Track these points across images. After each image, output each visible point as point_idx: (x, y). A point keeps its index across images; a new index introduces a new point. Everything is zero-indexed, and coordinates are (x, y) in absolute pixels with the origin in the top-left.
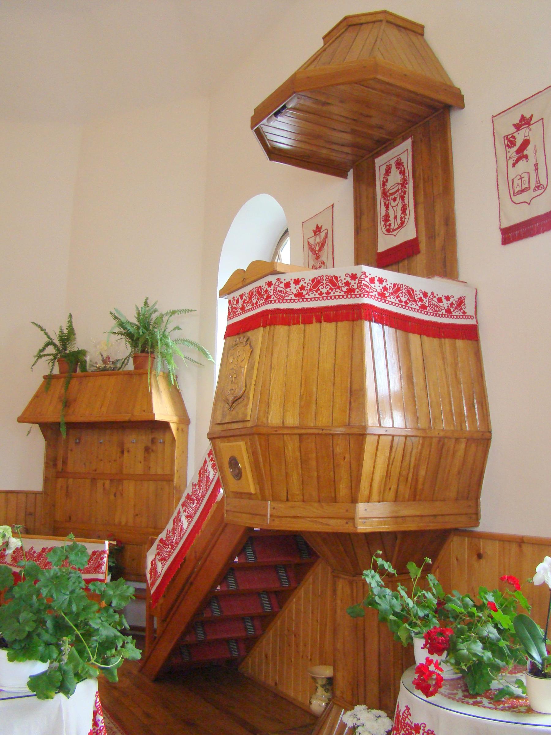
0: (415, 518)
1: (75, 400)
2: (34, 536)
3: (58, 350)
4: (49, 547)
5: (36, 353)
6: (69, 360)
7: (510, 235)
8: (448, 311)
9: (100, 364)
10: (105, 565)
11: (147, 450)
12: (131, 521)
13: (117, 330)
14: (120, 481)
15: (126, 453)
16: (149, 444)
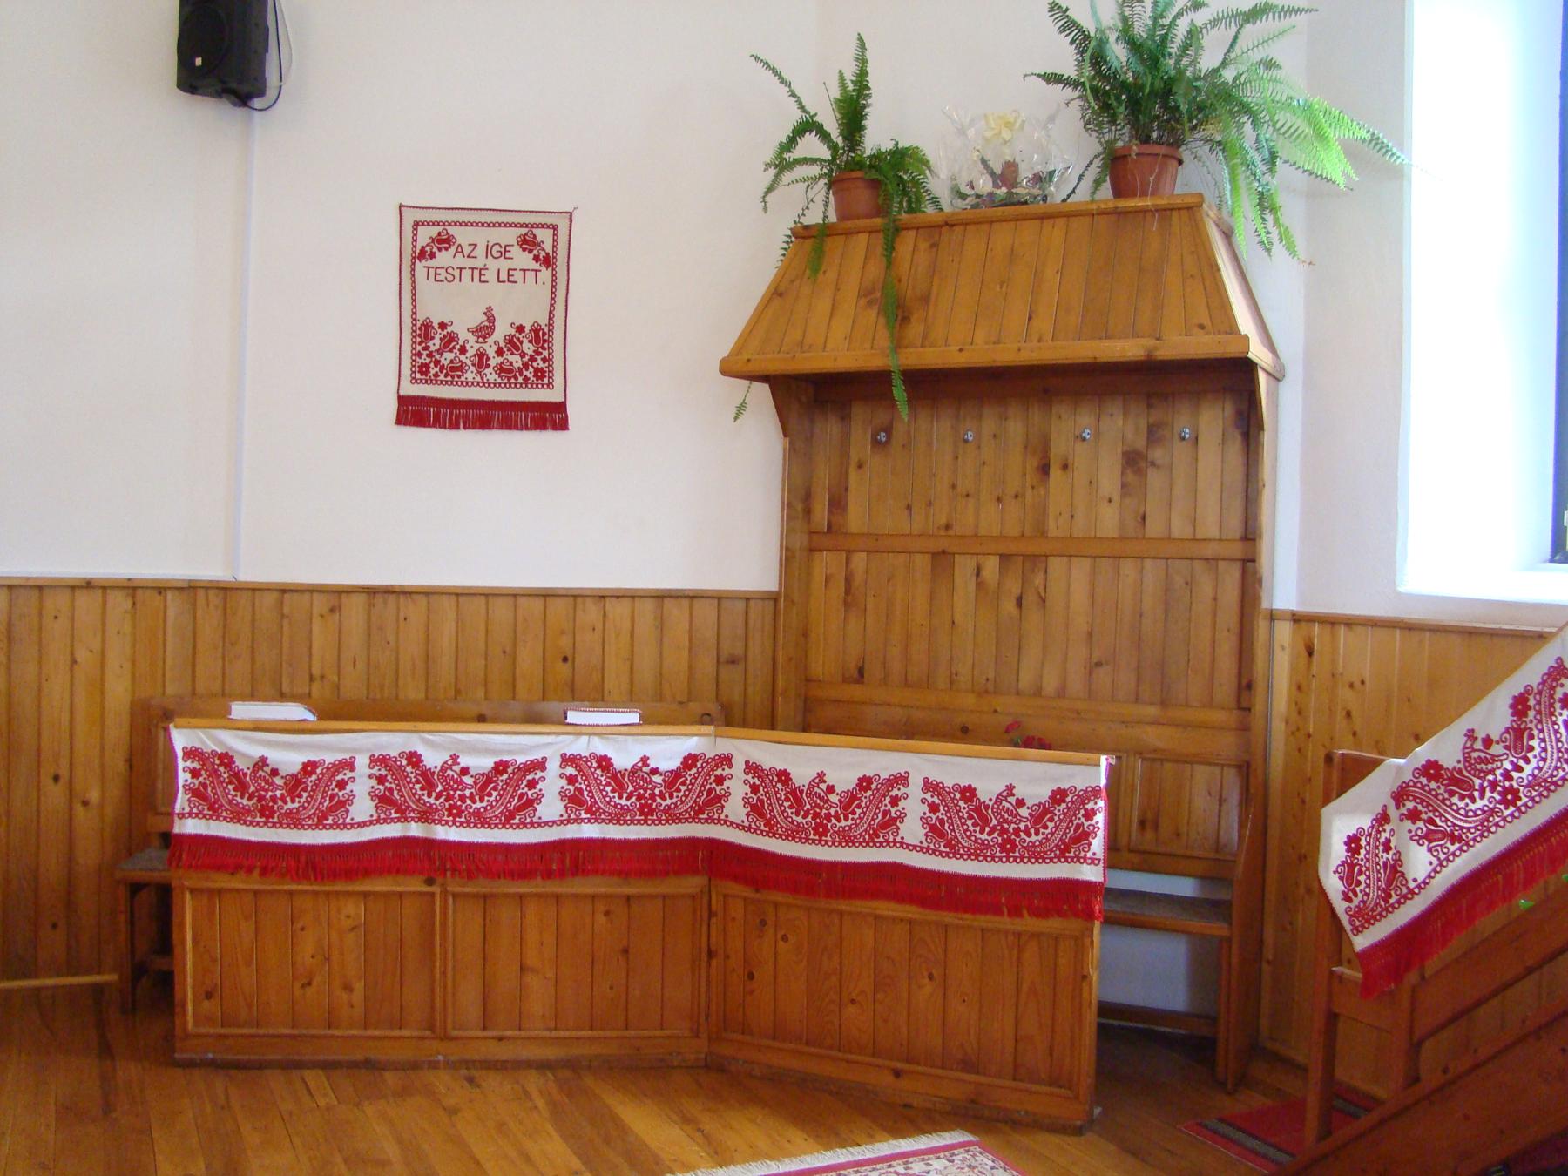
0: (685, 653)
1: (925, 299)
2: (744, 731)
3: (834, 148)
4: (884, 775)
5: (769, 154)
6: (869, 185)
9: (984, 185)
10: (1100, 834)
11: (1133, 461)
12: (1076, 685)
13: (1069, 69)
14: (1035, 561)
15: (1055, 472)
16: (1140, 443)
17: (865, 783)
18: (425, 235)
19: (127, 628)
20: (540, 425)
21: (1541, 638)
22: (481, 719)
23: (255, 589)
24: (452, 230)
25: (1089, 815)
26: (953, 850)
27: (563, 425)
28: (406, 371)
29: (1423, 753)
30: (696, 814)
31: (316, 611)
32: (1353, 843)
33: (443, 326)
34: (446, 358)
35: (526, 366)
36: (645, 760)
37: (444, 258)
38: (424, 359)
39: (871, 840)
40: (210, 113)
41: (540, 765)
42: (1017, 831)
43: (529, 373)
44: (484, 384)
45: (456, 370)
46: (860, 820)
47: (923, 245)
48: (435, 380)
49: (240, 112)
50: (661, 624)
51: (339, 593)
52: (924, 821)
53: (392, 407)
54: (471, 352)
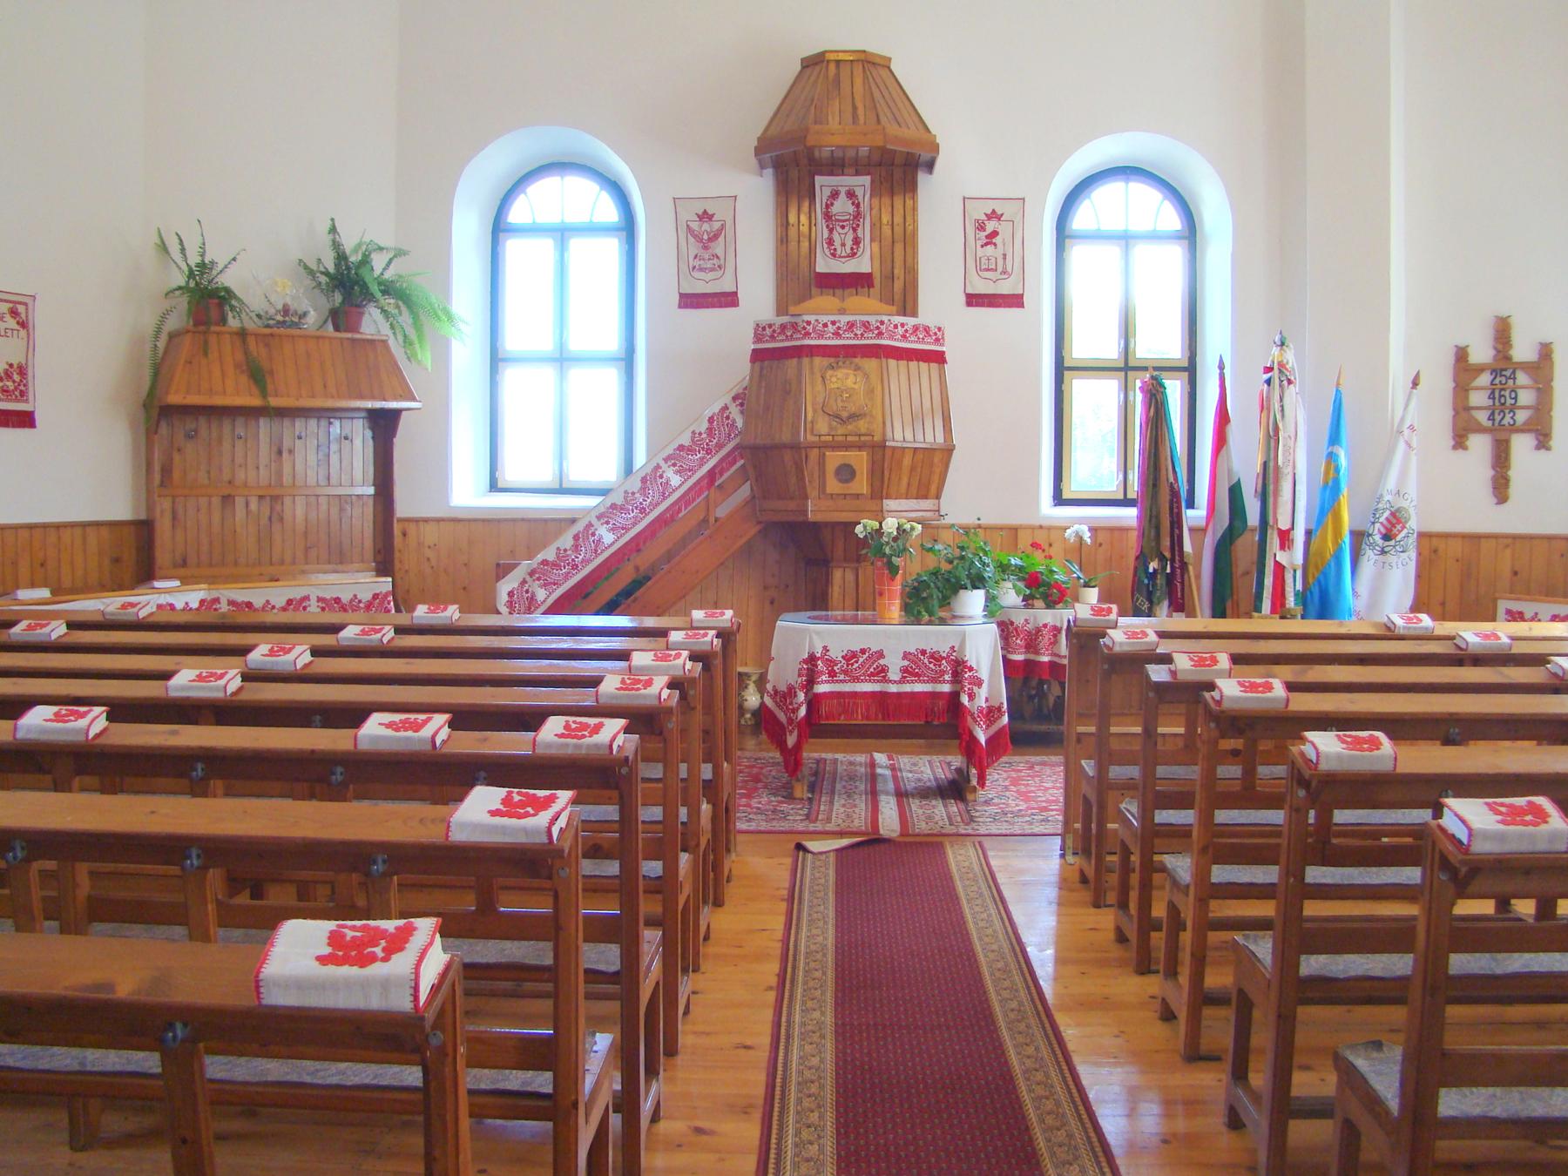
6: (207, 301)
7: (973, 300)
8: (904, 336)
15: (285, 454)
21: (574, 521)
29: (540, 557)
32: (511, 594)
50: (84, 538)
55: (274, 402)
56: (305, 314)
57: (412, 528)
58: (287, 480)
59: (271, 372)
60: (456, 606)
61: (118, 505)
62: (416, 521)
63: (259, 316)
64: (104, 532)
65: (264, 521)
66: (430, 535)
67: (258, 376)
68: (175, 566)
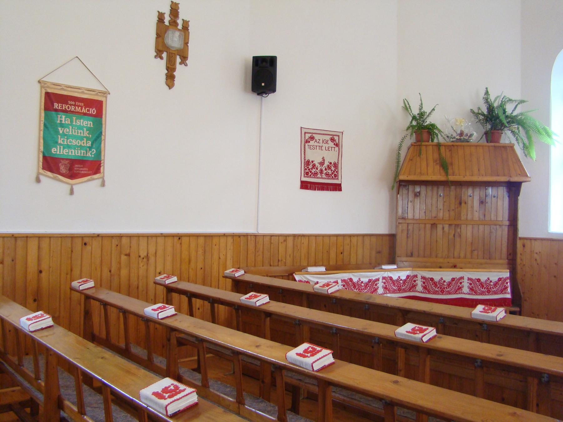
4: (458, 277)
15: (463, 204)
17: (453, 279)
18: (308, 136)
19: (232, 248)
20: (335, 189)
22: (440, 267)
23: (264, 236)
24: (314, 135)
25: (507, 283)
26: (476, 293)
27: (340, 190)
28: (303, 174)
30: (410, 290)
31: (280, 241)
33: (312, 162)
34: (313, 171)
35: (332, 173)
36: (399, 277)
37: (312, 143)
38: (307, 171)
39: (455, 293)
40: (255, 98)
41: (378, 280)
42: (491, 288)
43: (333, 175)
44: (322, 178)
45: (316, 174)
46: (453, 288)
47: (447, 150)
48: (310, 177)
49: (259, 97)
50: (363, 242)
51: (286, 236)
52: (469, 287)
53: (299, 184)
54: (319, 169)
55: (451, 178)
56: (471, 135)
57: (528, 243)
58: (463, 218)
59: (452, 164)
60: (328, 351)
61: (380, 225)
62: (530, 239)
63: (448, 137)
64: (374, 239)
65: (451, 236)
66: (537, 247)
67: (444, 166)
68: (407, 256)
